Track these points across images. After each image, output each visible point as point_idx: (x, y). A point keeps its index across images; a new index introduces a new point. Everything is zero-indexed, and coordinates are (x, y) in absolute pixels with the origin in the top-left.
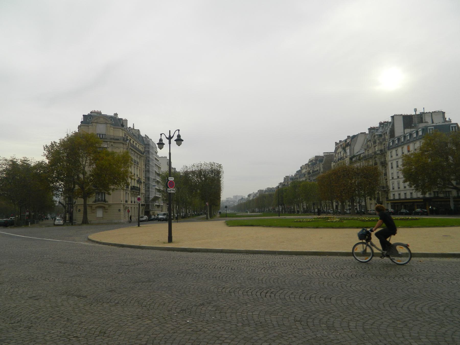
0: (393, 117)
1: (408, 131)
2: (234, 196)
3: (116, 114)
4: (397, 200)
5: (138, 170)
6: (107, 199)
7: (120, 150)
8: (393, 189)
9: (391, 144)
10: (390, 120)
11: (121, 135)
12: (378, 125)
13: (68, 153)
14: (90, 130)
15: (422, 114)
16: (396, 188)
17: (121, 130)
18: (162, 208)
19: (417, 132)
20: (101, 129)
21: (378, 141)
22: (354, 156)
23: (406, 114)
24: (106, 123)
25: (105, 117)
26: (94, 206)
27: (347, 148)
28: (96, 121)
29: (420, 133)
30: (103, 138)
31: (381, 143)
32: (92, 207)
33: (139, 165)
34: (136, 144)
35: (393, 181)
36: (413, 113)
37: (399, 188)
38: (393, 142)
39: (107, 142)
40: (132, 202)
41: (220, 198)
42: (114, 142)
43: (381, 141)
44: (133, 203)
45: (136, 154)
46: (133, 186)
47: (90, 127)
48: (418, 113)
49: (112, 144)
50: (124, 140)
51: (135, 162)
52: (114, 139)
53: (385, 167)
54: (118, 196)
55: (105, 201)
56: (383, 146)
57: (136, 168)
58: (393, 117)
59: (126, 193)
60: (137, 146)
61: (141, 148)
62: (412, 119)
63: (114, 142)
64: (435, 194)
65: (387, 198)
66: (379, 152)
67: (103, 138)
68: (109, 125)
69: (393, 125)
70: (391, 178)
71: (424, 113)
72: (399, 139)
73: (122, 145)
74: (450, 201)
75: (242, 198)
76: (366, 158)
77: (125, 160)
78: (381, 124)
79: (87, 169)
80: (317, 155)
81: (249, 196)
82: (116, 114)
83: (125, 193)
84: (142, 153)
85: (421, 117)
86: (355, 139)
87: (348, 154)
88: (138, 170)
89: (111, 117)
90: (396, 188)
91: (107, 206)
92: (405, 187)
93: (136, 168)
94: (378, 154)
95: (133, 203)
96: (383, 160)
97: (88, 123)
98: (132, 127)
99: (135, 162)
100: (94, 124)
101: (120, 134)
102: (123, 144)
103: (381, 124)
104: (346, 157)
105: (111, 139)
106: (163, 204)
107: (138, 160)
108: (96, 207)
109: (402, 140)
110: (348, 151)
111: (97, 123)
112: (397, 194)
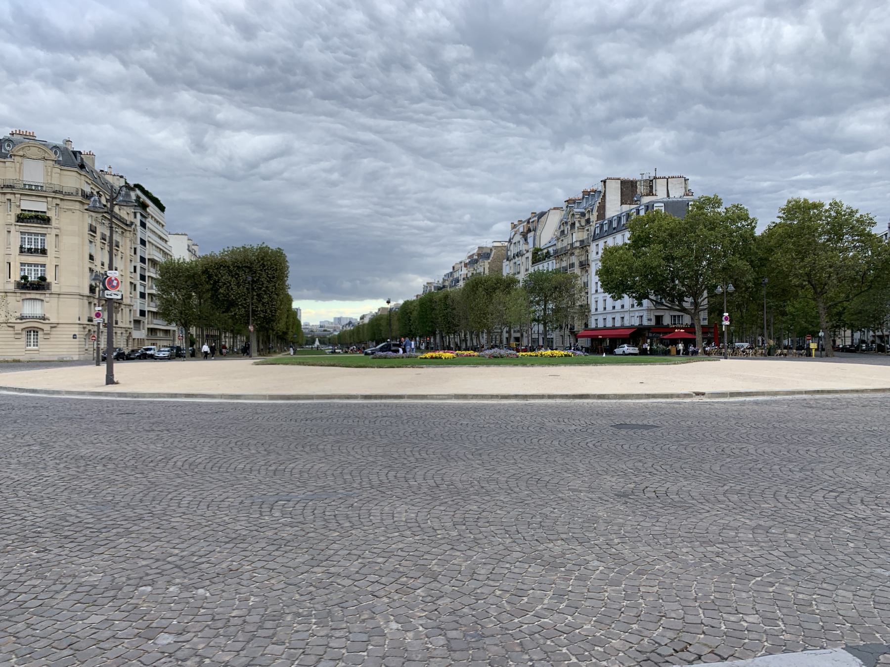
1: (626, 208)
2: (335, 319)
4: (618, 328)
8: (596, 309)
12: (581, 196)
16: (601, 309)
18: (174, 335)
19: (638, 211)
21: (577, 225)
24: (44, 159)
25: (44, 143)
27: (529, 235)
28: (21, 153)
29: (642, 213)
33: (121, 249)
35: (596, 296)
37: (605, 309)
38: (602, 226)
39: (46, 197)
41: (299, 322)
42: (62, 199)
43: (583, 224)
48: (646, 177)
49: (58, 201)
52: (61, 192)
53: (587, 271)
59: (90, 303)
61: (523, 116)
63: (62, 199)
66: (578, 244)
69: (604, 196)
70: (594, 291)
72: (611, 222)
73: (77, 206)
75: (350, 323)
76: (559, 255)
81: (362, 318)
83: (86, 302)
84: (127, 225)
87: (531, 245)
90: (601, 309)
91: (47, 328)
92: (614, 307)
94: (576, 248)
96: (583, 258)
100: (17, 159)
103: (585, 193)
104: (528, 252)
105: (55, 192)
106: (176, 329)
109: (615, 225)
110: (530, 240)
112: (600, 318)
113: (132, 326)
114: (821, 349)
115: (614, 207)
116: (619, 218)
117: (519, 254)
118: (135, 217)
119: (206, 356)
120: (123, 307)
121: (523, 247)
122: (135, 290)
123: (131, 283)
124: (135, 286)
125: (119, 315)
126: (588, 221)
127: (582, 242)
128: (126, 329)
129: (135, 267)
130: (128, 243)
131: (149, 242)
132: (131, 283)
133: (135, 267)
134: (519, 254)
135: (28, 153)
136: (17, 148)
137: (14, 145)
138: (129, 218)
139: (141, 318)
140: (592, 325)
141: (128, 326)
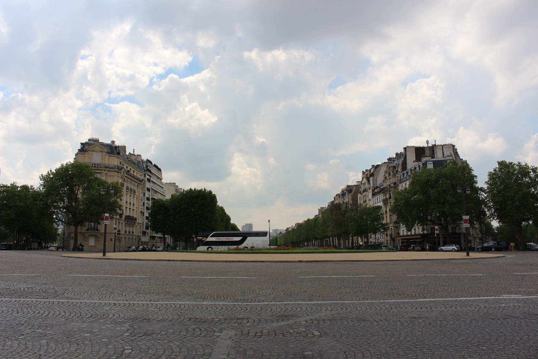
0: (405, 149)
3: (113, 142)
5: (135, 198)
6: (99, 228)
7: (112, 179)
9: (402, 178)
10: (403, 151)
11: (116, 164)
12: (394, 156)
13: (64, 180)
14: (86, 160)
15: (434, 146)
17: (116, 158)
20: (96, 158)
21: (392, 173)
22: (377, 188)
23: (418, 146)
24: (102, 152)
25: (102, 144)
26: (86, 235)
30: (95, 167)
31: (394, 176)
32: (84, 235)
33: (136, 194)
34: (134, 171)
36: (426, 145)
40: (126, 232)
42: (108, 171)
43: (395, 173)
44: (127, 233)
45: (133, 182)
46: (128, 216)
47: (86, 155)
48: (430, 145)
49: (107, 172)
50: (118, 168)
51: (131, 191)
52: (108, 167)
54: (110, 224)
55: (97, 230)
56: (396, 178)
57: (132, 197)
58: (405, 149)
59: (119, 222)
60: (135, 174)
62: (425, 151)
63: (108, 171)
64: (453, 230)
65: (399, 234)
66: (392, 185)
67: (97, 167)
68: (104, 153)
71: (435, 145)
73: (116, 174)
74: (460, 237)
75: (281, 233)
77: (117, 189)
78: (397, 154)
79: (79, 196)
80: (218, 198)
82: (113, 142)
84: (140, 181)
85: (433, 149)
86: (378, 169)
88: (135, 198)
89: (107, 145)
93: (132, 197)
94: (392, 187)
95: (127, 233)
97: (85, 151)
98: (132, 153)
99: (131, 191)
100: (90, 152)
101: (115, 161)
102: (118, 172)
103: (397, 154)
104: (370, 189)
105: (106, 167)
107: (136, 189)
108: (88, 236)
110: (371, 182)
111: (93, 151)
113: (141, 234)
114: (36, 247)
115: (411, 163)
116: (415, 168)
117: (365, 190)
118: (145, 176)
119: (134, 251)
120: (136, 224)
121: (367, 186)
122: (143, 215)
123: (141, 212)
124: (144, 213)
125: (134, 229)
126: (397, 172)
127: (395, 184)
128: (138, 236)
129: (144, 203)
130: (141, 191)
131: (152, 189)
132: (141, 212)
133: (144, 203)
134: (365, 190)
135: (95, 149)
136: (90, 147)
137: (89, 146)
138: (141, 177)
139: (146, 230)
140: (401, 234)
141: (139, 234)
